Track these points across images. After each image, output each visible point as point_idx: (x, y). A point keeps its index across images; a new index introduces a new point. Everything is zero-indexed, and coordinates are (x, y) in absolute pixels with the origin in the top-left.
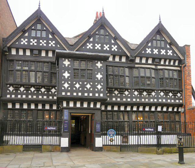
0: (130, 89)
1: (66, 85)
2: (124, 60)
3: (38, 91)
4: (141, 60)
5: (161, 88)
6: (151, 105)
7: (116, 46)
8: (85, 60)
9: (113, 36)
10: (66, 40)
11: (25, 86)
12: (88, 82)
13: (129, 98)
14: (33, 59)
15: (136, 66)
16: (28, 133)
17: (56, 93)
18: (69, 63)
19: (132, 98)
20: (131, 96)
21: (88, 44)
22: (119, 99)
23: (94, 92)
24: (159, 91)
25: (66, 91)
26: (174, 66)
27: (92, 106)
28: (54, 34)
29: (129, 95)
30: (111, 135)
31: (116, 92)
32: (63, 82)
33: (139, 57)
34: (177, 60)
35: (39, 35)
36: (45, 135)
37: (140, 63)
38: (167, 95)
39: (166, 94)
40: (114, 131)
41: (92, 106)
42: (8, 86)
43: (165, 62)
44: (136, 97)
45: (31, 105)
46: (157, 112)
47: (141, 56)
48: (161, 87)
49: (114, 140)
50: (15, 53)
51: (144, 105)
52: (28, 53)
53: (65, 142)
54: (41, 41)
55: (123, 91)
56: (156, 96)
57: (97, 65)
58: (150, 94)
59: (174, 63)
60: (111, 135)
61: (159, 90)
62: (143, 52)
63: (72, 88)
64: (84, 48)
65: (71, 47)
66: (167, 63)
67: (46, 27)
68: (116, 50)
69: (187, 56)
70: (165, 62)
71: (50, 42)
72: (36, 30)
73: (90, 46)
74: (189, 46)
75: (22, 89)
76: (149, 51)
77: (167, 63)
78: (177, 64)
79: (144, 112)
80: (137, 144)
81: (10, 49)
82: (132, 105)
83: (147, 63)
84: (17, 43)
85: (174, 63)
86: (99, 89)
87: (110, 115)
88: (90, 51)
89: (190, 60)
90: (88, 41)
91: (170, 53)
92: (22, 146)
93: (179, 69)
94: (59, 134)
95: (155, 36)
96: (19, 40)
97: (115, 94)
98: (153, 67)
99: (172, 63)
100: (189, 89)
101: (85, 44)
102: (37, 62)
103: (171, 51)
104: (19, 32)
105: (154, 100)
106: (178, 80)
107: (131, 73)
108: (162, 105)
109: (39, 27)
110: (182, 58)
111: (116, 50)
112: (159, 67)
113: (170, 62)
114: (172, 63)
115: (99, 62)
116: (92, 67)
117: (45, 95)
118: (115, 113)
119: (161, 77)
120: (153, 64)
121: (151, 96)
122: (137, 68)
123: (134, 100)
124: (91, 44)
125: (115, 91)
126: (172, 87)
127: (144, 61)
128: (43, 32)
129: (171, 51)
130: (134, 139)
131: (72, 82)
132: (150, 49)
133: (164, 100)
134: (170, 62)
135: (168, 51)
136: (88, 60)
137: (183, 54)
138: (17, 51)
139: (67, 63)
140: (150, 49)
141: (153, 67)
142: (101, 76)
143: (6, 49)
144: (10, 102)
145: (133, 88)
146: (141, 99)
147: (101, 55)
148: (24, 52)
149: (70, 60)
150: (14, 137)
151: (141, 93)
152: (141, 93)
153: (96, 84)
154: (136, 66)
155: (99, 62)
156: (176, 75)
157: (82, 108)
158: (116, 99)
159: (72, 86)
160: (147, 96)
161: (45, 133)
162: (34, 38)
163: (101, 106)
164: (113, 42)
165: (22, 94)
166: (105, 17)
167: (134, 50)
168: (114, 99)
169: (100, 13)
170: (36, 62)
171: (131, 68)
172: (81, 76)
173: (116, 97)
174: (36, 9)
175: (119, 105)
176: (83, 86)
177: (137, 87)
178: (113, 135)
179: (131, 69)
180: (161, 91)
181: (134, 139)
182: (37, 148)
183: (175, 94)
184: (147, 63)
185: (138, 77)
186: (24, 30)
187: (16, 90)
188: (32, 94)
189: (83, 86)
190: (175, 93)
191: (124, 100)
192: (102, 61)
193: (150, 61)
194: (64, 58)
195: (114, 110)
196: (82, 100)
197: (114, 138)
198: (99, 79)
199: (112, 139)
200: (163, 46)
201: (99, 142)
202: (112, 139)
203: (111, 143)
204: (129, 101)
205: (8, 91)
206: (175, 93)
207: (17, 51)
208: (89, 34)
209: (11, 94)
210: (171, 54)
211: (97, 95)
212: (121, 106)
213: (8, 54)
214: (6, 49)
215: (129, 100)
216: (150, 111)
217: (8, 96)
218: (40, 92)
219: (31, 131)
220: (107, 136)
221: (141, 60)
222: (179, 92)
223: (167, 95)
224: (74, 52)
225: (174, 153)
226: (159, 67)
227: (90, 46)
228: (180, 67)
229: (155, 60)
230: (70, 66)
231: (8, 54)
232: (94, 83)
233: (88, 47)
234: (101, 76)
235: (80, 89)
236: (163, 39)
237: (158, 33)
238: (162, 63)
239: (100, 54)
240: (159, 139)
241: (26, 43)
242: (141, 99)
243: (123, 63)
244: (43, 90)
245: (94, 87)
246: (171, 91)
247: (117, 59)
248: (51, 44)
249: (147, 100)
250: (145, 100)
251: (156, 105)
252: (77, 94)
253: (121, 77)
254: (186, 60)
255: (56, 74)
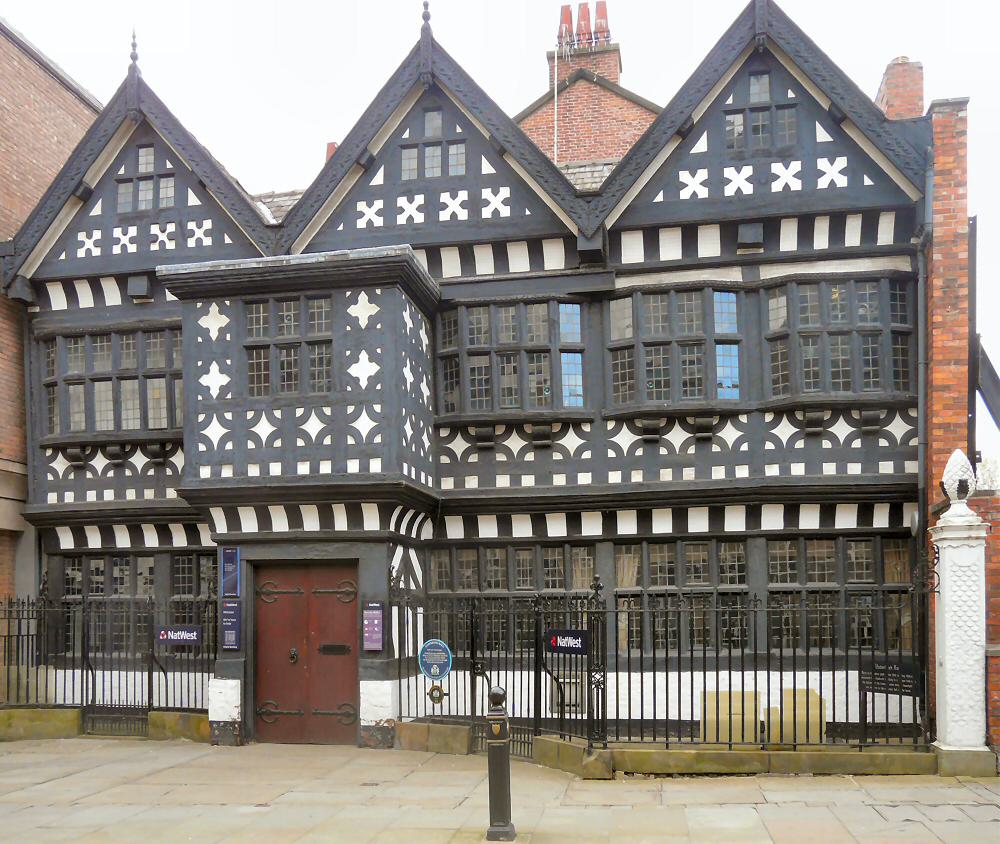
0: (591, 421)
1: (215, 431)
2: (554, 258)
3: (543, 452)
4: (651, 243)
5: (774, 398)
6: (716, 501)
7: (505, 192)
8: (295, 294)
9: (825, 105)
10: (566, 180)
11: (799, 416)
12: (314, 406)
13: (585, 466)
14: (135, 319)
15: (622, 283)
16: (800, 652)
17: (914, 442)
18: (224, 321)
19: (599, 467)
20: (598, 454)
21: (361, 206)
22: (528, 481)
23: (289, 457)
24: (769, 417)
25: (217, 459)
26: (868, 250)
27: (341, 523)
28: (844, 118)
29: (587, 455)
30: (435, 670)
31: (515, 443)
32: (201, 418)
33: (793, 217)
34: (888, 209)
35: (433, 171)
36: (518, 665)
37: (653, 267)
38: (119, 467)
39: (813, 428)
40: (444, 650)
41: (341, 523)
42: (49, 452)
43: (806, 234)
44: (626, 463)
45: (798, 512)
46: (763, 540)
47: (648, 222)
48: (836, 386)
49: (448, 695)
50: (64, 306)
51: (680, 502)
52: (113, 296)
53: (223, 698)
54: (155, 229)
55: (656, 431)
56: (744, 447)
57: (353, 310)
58: (708, 440)
59: (870, 230)
60: (435, 670)
61: (764, 411)
62: (660, 198)
63: (240, 445)
64: (341, 228)
65: (269, 232)
66: (821, 241)
67: (798, 88)
68: (505, 212)
69: (941, 173)
70: (806, 234)
71: (191, 225)
72: (420, 145)
73: (370, 214)
74: (961, 104)
75: (677, 436)
76: (694, 185)
77: (821, 241)
78: (886, 235)
79: (684, 539)
80: (855, 718)
81: (38, 286)
82: (609, 506)
83: (691, 262)
84: (63, 257)
85: (870, 230)
86: (364, 435)
87: (496, 562)
88: (372, 235)
89: (964, 196)
90: (682, 159)
91: (833, 173)
92: (73, 714)
93: (903, 265)
94: (203, 658)
95: (414, 119)
96: (68, 241)
97: (508, 451)
98: (734, 275)
99: (853, 237)
100: (947, 388)
101: (347, 212)
102: (146, 331)
103: (842, 162)
104: (665, 137)
105: (730, 472)
106: (886, 339)
107: (594, 327)
108: (791, 498)
109: (146, 161)
110: (913, 195)
111: (505, 212)
112: (769, 273)
113: (837, 232)
114: (853, 237)
115: (363, 297)
116: (329, 327)
117: (854, 456)
118: (525, 556)
119: (869, 325)
120: (728, 258)
121: (663, 451)
122: (628, 293)
123: (615, 477)
124: (703, 174)
125: (507, 434)
126: (847, 386)
127: (671, 248)
128: (163, 182)
129: (842, 162)
130: (686, 691)
131: (240, 417)
132: (703, 174)
133: (798, 469)
134: (837, 232)
135: (822, 164)
136: (309, 293)
137: (918, 166)
138: (71, 294)
139: (214, 321)
140: (703, 174)
141: (734, 275)
142: (225, 380)
143: (27, 295)
144: (594, 509)
145: (606, 412)
146: (652, 472)
147: (362, 256)
148: (98, 292)
149: (228, 303)
150: (518, 673)
151: (651, 437)
152: (651, 437)
153: (350, 409)
154: (622, 283)
155: (363, 297)
156: (869, 312)
157: (328, 536)
158: (516, 480)
159: (240, 431)
160: (692, 450)
161: (69, 655)
162: (125, 221)
163: (384, 520)
164: (822, 136)
165: (516, 467)
166: (433, 39)
167: (595, 194)
168: (503, 481)
169: (584, 10)
170: (167, 332)
171: (595, 301)
172: (296, 376)
173: (516, 467)
174: (122, 75)
175: (538, 509)
176: (289, 429)
177: (630, 407)
178: (443, 668)
179: (598, 305)
180: (781, 412)
181: (686, 691)
182: (114, 720)
183: (869, 427)
184: (689, 261)
185: (632, 347)
186: (689, 124)
187: (646, 441)
188: (140, 481)
189: (289, 429)
190: (869, 421)
191: (559, 480)
192: (378, 285)
193: (709, 245)
194: (349, 287)
195: (654, 532)
196: (292, 496)
197: (445, 680)
198: (364, 384)
199: (439, 689)
200: (458, 168)
201: (377, 699)
202: (439, 689)
203: (437, 706)
204: (588, 486)
205: (50, 477)
206: (869, 421)
207: (71, 294)
208: (684, 117)
209: (60, 487)
210: (842, 182)
211: (353, 466)
212: (802, 506)
213: (37, 309)
214: (27, 295)
215: (585, 479)
216: (506, 543)
217: (52, 498)
218: (169, 472)
219: (744, 645)
220: (421, 677)
221: (651, 243)
222: (900, 408)
223: (119, 467)
224: (297, 258)
225: (682, 775)
226: (769, 273)
227: (370, 214)
228: (911, 253)
229: (736, 234)
230: (228, 337)
231: (37, 309)
232: (339, 405)
233: (361, 224)
234: (225, 380)
235: (278, 443)
236: (791, 94)
237: (144, 141)
238: (788, 241)
239: (353, 254)
240: (445, 694)
241: (96, 252)
242: (652, 472)
243: (555, 276)
244: (841, 429)
245: (338, 426)
246: (841, 410)
247: (485, 264)
248: (91, 246)
249: (69, 497)
250: (678, 473)
251: (753, 499)
252: (265, 470)
253: (531, 360)
254: (933, 205)
255: (911, 339)
